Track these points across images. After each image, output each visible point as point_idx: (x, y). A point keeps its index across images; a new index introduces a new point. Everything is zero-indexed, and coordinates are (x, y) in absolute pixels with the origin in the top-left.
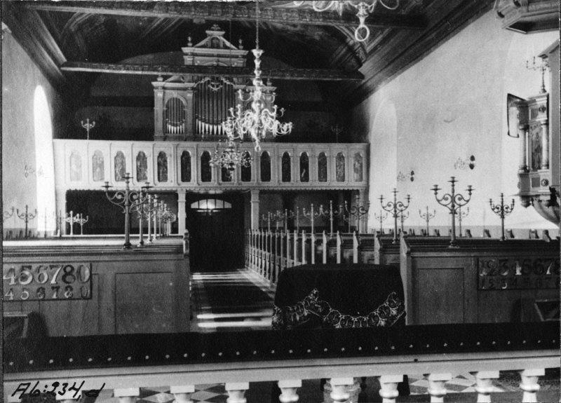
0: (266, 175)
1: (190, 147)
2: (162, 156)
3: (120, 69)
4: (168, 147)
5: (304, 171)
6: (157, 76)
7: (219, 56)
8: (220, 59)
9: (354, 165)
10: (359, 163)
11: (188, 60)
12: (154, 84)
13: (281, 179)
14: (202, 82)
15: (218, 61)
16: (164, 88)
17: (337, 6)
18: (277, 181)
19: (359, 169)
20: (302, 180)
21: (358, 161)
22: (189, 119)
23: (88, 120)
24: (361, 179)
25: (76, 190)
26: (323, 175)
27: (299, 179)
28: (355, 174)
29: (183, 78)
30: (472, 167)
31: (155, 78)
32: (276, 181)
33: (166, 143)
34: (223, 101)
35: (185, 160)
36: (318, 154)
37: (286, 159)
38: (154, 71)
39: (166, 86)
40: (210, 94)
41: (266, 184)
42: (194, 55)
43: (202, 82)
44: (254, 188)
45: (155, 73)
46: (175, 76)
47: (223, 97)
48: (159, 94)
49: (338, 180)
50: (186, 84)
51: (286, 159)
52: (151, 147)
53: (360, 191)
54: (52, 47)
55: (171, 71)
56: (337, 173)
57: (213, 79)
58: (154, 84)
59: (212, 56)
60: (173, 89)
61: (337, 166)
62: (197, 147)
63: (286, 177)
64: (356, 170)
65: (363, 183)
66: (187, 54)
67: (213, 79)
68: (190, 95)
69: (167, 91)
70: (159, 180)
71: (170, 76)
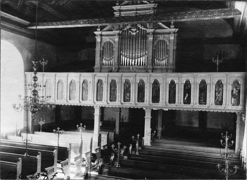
0: (156, 98)
1: (115, 76)
2: (219, 84)
3: (58, 25)
4: (103, 76)
5: (187, 95)
6: (97, 27)
7: (137, 10)
8: (138, 12)
9: (232, 91)
10: (237, 89)
11: (117, 14)
12: (95, 33)
13: (167, 101)
14: (125, 29)
15: (137, 13)
16: (101, 35)
17: (0, 5)
18: (164, 102)
19: (237, 94)
20: (184, 103)
21: (236, 88)
22: (116, 55)
23: (44, 60)
24: (238, 104)
25: (90, 106)
26: (203, 99)
27: (182, 101)
28: (233, 99)
29: (113, 27)
30: (50, 97)
31: (95, 29)
32: (163, 104)
33: (102, 74)
34: (140, 41)
35: (113, 85)
36: (199, 81)
37: (172, 86)
38: (78, 24)
39: (102, 34)
40: (131, 37)
41: (155, 105)
42: (120, 11)
43: (125, 29)
44: (147, 108)
45: (95, 25)
46: (109, 26)
47: (140, 39)
48: (98, 39)
49: (216, 104)
50: (114, 31)
51: (172, 86)
52: (79, 76)
53: (237, 114)
54: (14, 19)
55: (106, 22)
56: (216, 97)
57: (133, 26)
58: (95, 33)
59: (133, 10)
60: (107, 35)
61: (216, 92)
62: (108, 77)
63: (172, 100)
64: (233, 95)
65: (240, 108)
66: (116, 11)
67: (133, 26)
68: (117, 39)
69: (103, 37)
70: (97, 100)
71: (105, 27)
